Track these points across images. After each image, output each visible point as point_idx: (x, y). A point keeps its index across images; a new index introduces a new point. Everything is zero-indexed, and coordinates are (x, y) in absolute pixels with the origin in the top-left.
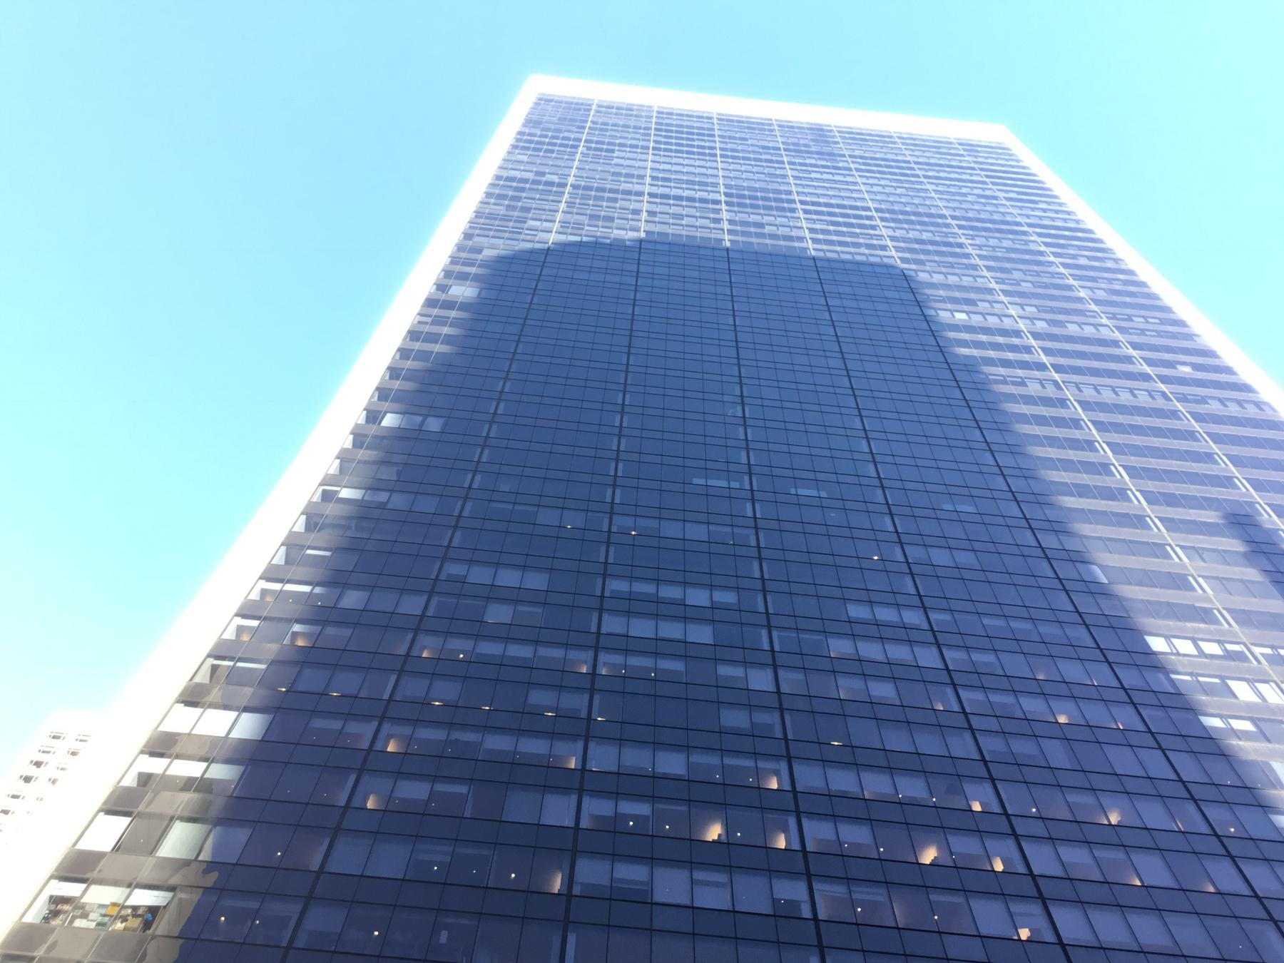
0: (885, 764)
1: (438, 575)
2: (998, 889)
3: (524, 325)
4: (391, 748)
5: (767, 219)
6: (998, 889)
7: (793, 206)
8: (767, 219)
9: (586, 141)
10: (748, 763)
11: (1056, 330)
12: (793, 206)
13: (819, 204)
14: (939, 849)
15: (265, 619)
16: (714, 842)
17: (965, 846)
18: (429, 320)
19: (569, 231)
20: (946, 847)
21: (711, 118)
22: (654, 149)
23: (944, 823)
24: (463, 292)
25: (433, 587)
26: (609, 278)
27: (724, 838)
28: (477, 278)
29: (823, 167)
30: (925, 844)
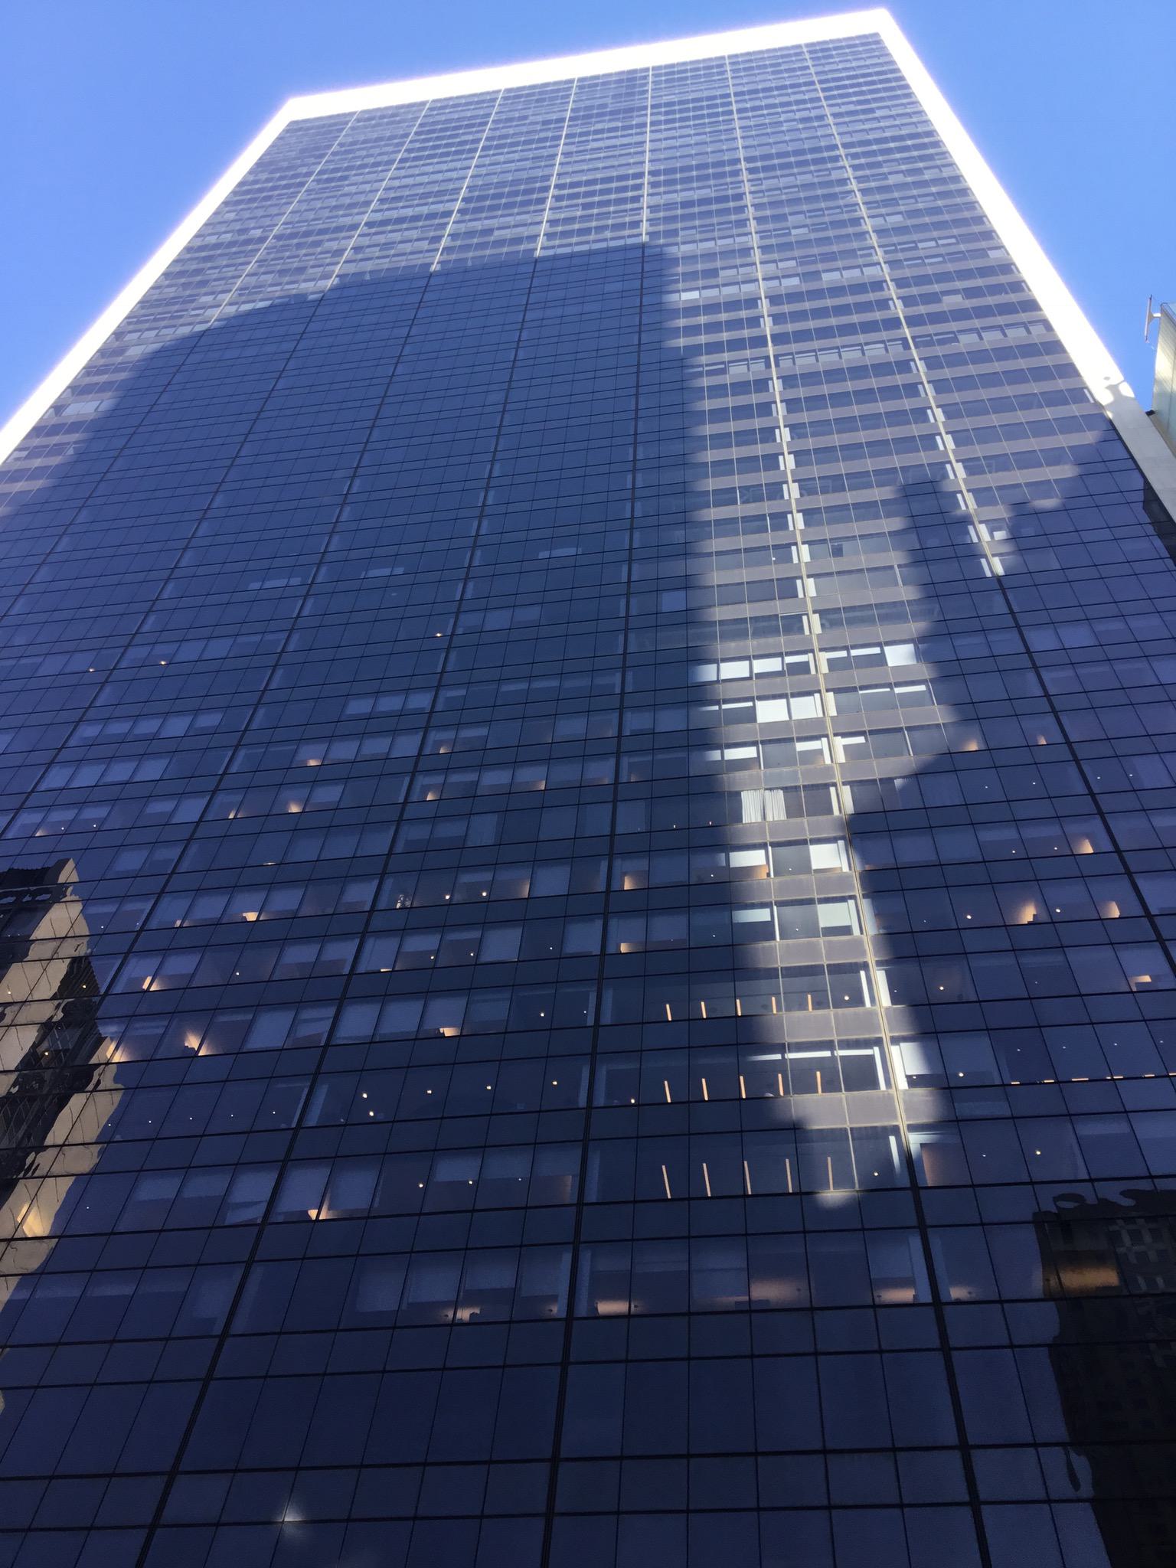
0: (1139, 807)
1: (623, 688)
2: (1112, 937)
3: (638, 372)
4: (628, 885)
5: (494, 223)
6: (1112, 937)
7: (836, 153)
8: (494, 223)
9: (653, 123)
10: (1052, 830)
11: (813, 286)
12: (836, 153)
13: (868, 143)
14: (1036, 907)
15: (872, 732)
16: (1030, 924)
17: (1067, 899)
18: (25, 453)
19: (716, 234)
20: (1045, 904)
21: (721, 66)
22: (739, 111)
23: (1030, 873)
24: (88, 408)
25: (429, 721)
26: (587, 308)
27: (1045, 918)
28: (675, 313)
29: (610, 130)
30: (1023, 901)
